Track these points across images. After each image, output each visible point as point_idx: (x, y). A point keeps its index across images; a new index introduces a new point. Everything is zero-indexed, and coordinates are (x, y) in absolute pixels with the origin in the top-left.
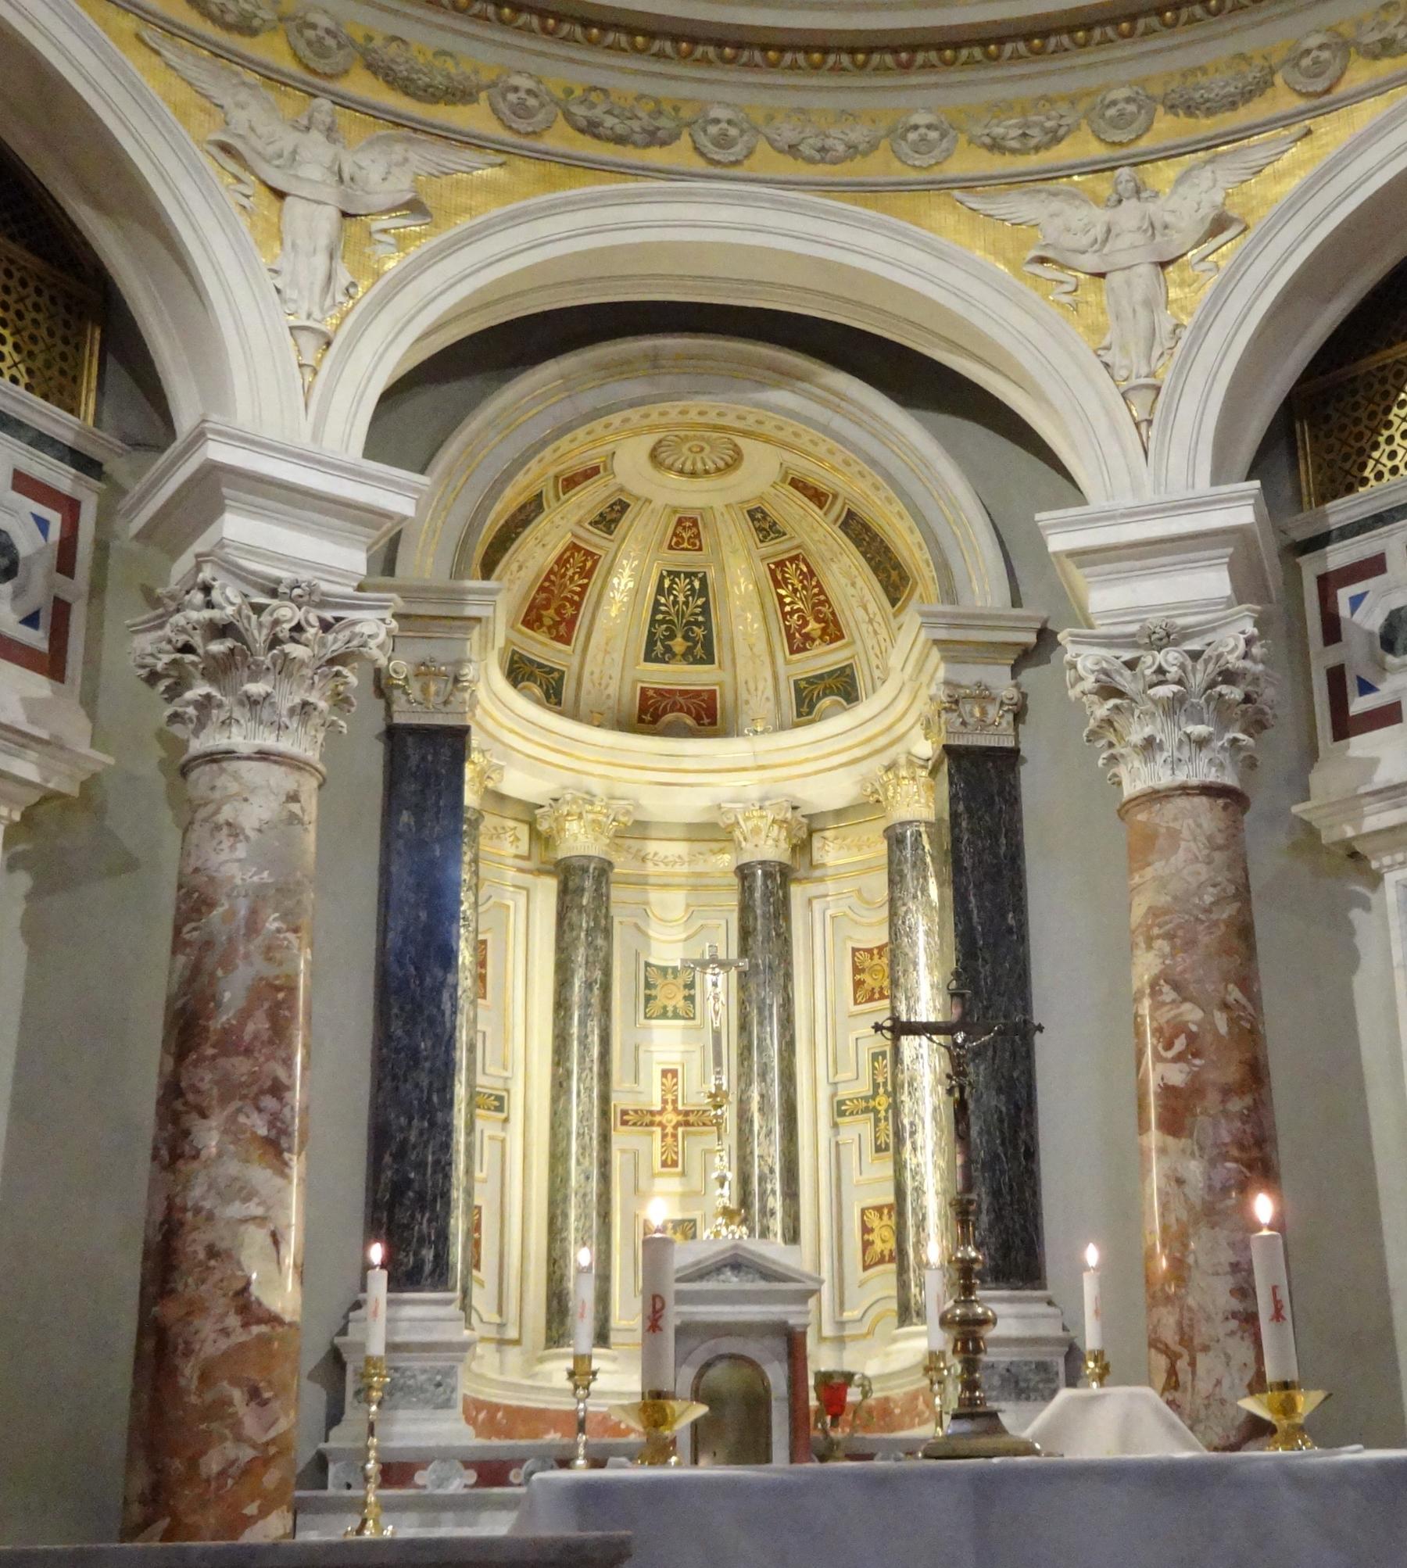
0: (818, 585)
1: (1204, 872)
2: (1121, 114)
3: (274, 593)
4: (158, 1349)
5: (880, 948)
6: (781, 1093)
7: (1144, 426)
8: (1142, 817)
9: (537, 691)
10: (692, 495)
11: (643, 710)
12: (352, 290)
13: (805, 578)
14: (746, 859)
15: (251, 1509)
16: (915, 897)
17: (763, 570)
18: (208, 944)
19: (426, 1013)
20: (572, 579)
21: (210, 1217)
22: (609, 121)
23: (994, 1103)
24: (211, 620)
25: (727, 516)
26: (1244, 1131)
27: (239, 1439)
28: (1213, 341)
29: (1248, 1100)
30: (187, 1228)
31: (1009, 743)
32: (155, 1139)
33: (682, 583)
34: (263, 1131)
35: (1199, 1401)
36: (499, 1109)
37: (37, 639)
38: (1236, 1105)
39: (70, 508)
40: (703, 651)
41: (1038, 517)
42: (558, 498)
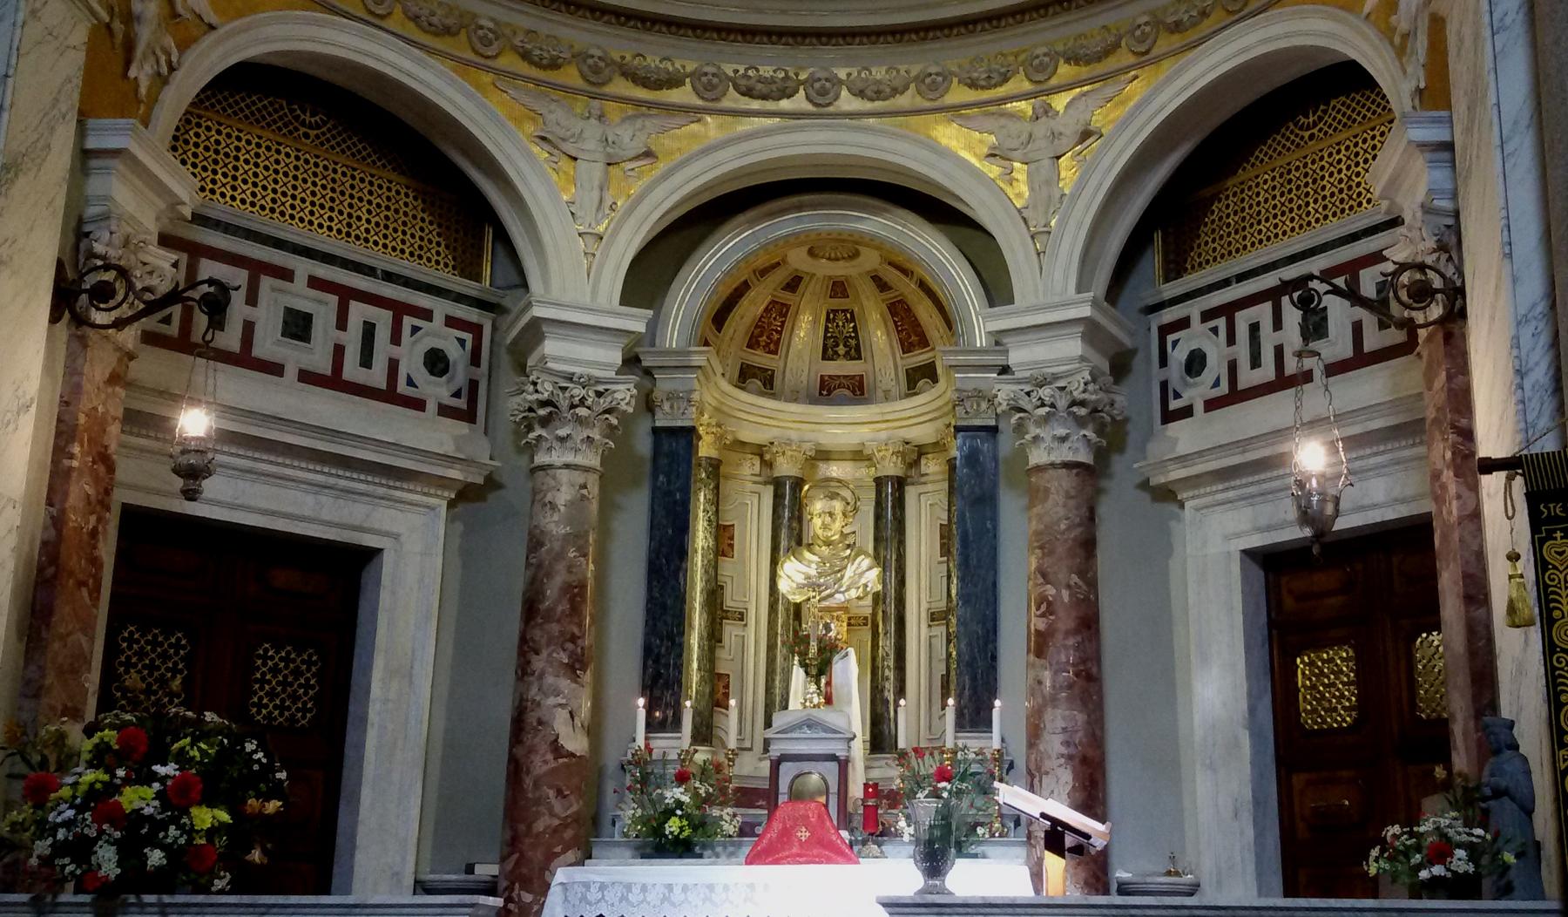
1: (1061, 512)
2: (1041, 63)
3: (571, 380)
4: (516, 770)
10: (840, 269)
11: (822, 387)
15: (558, 849)
18: (540, 566)
21: (539, 704)
22: (759, 86)
27: (552, 815)
28: (1081, 204)
33: (841, 315)
36: (742, 619)
37: (461, 403)
39: (476, 329)
40: (855, 353)
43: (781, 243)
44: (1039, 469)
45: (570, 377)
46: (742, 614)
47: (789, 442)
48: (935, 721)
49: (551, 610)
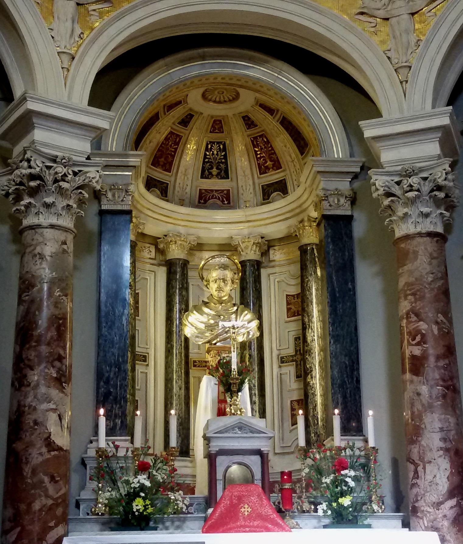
0: (271, 146)
1: (428, 268)
3: (55, 161)
5: (298, 295)
6: (257, 354)
7: (404, 83)
8: (403, 245)
9: (158, 192)
11: (200, 197)
12: (81, 36)
13: (265, 143)
14: (243, 259)
15: (52, 524)
16: (311, 275)
17: (248, 140)
18: (32, 301)
19: (116, 325)
20: (171, 146)
21: (35, 409)
23: (344, 360)
24: (30, 173)
25: (234, 119)
26: (445, 374)
28: (434, 46)
29: (447, 361)
30: (26, 414)
31: (349, 213)
32: (12, 378)
33: (215, 146)
34: (55, 375)
35: (427, 483)
38: (441, 363)
40: (224, 174)
41: (360, 123)
42: (165, 114)
43: (188, 83)
44: (407, 237)
45: (54, 160)
46: (145, 357)
47: (179, 235)
48: (287, 434)
49: (40, 336)
